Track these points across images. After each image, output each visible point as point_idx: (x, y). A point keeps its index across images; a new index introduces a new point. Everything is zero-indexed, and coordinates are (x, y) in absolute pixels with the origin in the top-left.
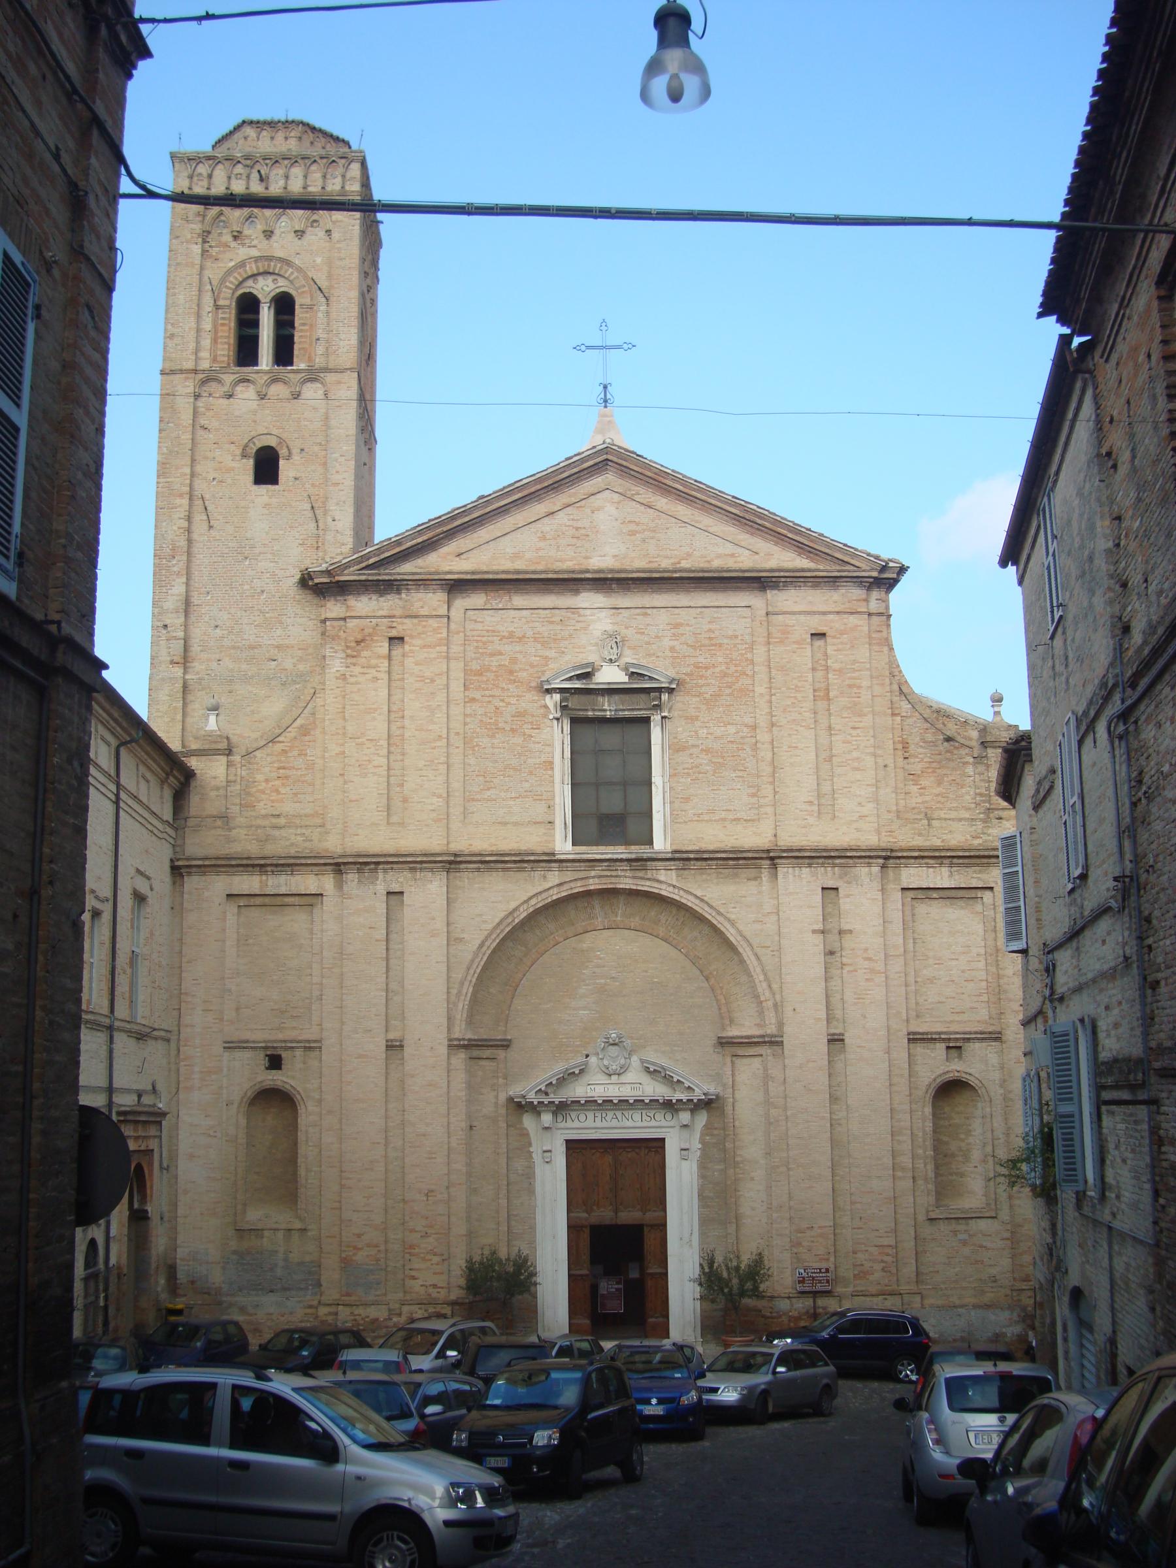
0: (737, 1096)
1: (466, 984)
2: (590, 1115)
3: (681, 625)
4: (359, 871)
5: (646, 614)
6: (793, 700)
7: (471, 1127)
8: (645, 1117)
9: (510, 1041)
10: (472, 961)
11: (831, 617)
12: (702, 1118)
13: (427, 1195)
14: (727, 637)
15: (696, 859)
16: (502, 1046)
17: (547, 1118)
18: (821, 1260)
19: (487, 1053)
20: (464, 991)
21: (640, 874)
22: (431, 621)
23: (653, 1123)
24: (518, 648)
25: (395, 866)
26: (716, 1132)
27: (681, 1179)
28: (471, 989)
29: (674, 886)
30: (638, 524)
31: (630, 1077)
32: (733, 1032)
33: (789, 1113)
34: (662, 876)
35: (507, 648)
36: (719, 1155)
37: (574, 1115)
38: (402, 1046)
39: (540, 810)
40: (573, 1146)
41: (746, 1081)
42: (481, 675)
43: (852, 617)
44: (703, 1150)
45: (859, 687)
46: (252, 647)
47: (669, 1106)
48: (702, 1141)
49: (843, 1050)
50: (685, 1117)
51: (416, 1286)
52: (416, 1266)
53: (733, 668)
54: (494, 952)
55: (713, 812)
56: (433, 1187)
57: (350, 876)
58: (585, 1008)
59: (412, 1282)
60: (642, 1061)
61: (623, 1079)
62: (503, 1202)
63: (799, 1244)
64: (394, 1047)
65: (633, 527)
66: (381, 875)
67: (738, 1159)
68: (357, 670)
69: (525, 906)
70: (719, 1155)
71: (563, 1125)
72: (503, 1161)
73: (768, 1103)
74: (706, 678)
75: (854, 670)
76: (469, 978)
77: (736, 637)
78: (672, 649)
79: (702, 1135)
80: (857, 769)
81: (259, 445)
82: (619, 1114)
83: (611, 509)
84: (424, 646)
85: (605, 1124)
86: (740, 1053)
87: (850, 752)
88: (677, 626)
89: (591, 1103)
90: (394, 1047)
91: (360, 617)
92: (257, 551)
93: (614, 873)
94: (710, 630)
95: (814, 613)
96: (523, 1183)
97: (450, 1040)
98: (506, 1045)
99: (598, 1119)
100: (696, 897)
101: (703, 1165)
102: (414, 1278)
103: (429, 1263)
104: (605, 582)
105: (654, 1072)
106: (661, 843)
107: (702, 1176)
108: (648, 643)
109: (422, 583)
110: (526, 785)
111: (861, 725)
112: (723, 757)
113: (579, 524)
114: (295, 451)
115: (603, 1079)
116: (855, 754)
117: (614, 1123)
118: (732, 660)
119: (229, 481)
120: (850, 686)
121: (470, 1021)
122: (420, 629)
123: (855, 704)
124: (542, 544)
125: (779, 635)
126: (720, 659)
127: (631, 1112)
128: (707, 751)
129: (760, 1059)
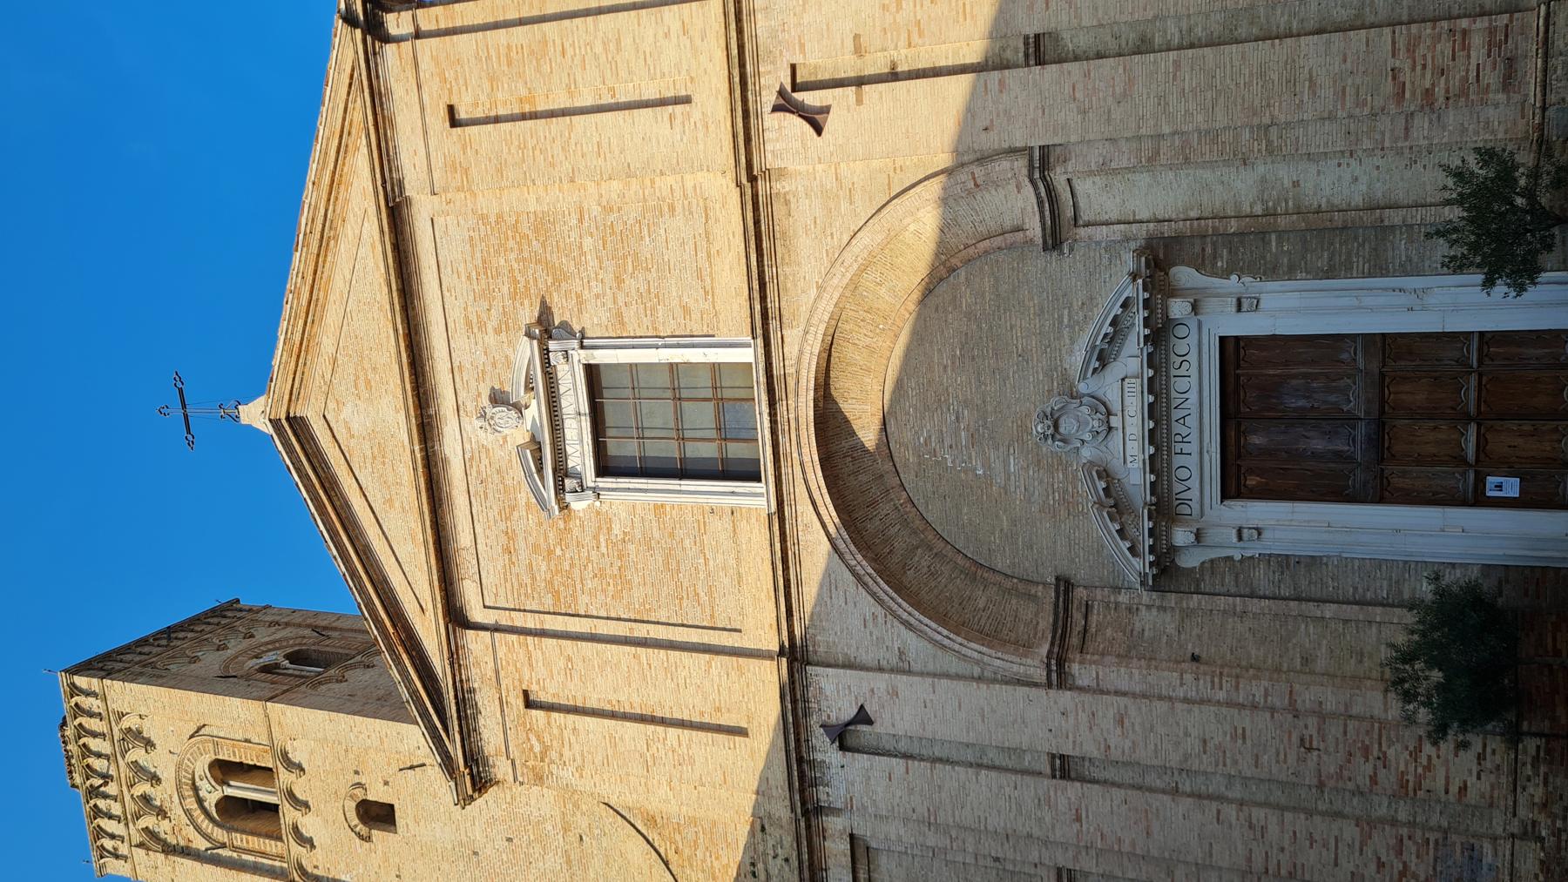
0: (1144, 215)
1: (964, 651)
2: (1178, 461)
3: (466, 317)
4: (815, 783)
5: (460, 367)
6: (537, 152)
7: (1195, 658)
8: (1182, 372)
9: (1057, 579)
10: (931, 640)
11: (426, 97)
12: (1184, 275)
13: (1310, 749)
14: (473, 253)
15: (763, 298)
16: (1066, 592)
17: (1181, 536)
18: (1466, 47)
19: (1078, 617)
20: (975, 655)
21: (791, 383)
22: (500, 654)
23: (1193, 357)
24: (522, 544)
25: (803, 738)
26: (1209, 250)
27: (1288, 309)
28: (973, 645)
29: (806, 333)
30: (357, 378)
31: (1112, 396)
32: (1035, 229)
33: (1166, 130)
34: (791, 350)
35: (523, 555)
36: (1249, 245)
37: (1178, 487)
38: (1062, 757)
39: (719, 526)
40: (1232, 489)
41: (1124, 200)
42: (558, 592)
43: (422, 66)
44: (1241, 273)
45: (509, 47)
46: (569, 862)
47: (1160, 334)
48: (1226, 275)
49: (1054, 36)
50: (1178, 308)
51: (1478, 788)
52: (1440, 783)
53: (511, 243)
54: (917, 605)
55: (699, 271)
56: (1295, 739)
57: (823, 797)
58: (1006, 464)
59: (1472, 796)
60: (1083, 377)
61: (1116, 406)
62: (1329, 610)
63: (1428, 93)
64: (1064, 768)
65: (361, 384)
66: (819, 757)
67: (1258, 210)
68: (567, 753)
69: (848, 556)
70: (1249, 245)
71: (1195, 505)
72: (1255, 605)
73: (1151, 162)
74: (527, 282)
75: (488, 57)
76: (957, 647)
77: (471, 238)
78: (498, 331)
79: (1214, 274)
80: (618, 42)
81: (355, 821)
82: (1176, 414)
83: (346, 412)
84: (531, 665)
85: (1194, 437)
86: (1069, 213)
87: (596, 58)
88: (469, 324)
89: (1158, 464)
90: (1064, 768)
91: (506, 741)
92: (465, 839)
93: (793, 425)
94: (469, 278)
95: (424, 124)
96: (1298, 575)
97: (1049, 685)
98: (1065, 586)
99: (1186, 448)
100: (819, 297)
101: (1270, 271)
102: (1463, 789)
103: (1435, 760)
104: (426, 428)
105: (1103, 358)
106: (746, 355)
107: (1290, 273)
108: (494, 365)
109: (455, 657)
110: (687, 543)
111: (558, 42)
112: (625, 257)
113: (369, 453)
114: (357, 779)
115: (1117, 437)
116: (599, 49)
117: (1192, 421)
118: (500, 245)
119: (397, 860)
120: (509, 64)
121: (1024, 647)
122: (512, 668)
123: (532, 52)
124: (397, 504)
125: (458, 176)
126: (502, 262)
127: (1174, 394)
128: (619, 280)
129: (1075, 182)
